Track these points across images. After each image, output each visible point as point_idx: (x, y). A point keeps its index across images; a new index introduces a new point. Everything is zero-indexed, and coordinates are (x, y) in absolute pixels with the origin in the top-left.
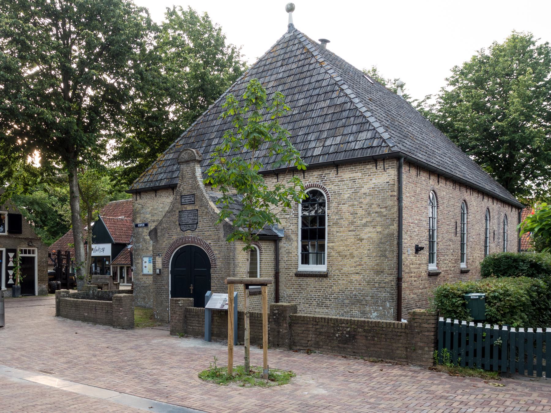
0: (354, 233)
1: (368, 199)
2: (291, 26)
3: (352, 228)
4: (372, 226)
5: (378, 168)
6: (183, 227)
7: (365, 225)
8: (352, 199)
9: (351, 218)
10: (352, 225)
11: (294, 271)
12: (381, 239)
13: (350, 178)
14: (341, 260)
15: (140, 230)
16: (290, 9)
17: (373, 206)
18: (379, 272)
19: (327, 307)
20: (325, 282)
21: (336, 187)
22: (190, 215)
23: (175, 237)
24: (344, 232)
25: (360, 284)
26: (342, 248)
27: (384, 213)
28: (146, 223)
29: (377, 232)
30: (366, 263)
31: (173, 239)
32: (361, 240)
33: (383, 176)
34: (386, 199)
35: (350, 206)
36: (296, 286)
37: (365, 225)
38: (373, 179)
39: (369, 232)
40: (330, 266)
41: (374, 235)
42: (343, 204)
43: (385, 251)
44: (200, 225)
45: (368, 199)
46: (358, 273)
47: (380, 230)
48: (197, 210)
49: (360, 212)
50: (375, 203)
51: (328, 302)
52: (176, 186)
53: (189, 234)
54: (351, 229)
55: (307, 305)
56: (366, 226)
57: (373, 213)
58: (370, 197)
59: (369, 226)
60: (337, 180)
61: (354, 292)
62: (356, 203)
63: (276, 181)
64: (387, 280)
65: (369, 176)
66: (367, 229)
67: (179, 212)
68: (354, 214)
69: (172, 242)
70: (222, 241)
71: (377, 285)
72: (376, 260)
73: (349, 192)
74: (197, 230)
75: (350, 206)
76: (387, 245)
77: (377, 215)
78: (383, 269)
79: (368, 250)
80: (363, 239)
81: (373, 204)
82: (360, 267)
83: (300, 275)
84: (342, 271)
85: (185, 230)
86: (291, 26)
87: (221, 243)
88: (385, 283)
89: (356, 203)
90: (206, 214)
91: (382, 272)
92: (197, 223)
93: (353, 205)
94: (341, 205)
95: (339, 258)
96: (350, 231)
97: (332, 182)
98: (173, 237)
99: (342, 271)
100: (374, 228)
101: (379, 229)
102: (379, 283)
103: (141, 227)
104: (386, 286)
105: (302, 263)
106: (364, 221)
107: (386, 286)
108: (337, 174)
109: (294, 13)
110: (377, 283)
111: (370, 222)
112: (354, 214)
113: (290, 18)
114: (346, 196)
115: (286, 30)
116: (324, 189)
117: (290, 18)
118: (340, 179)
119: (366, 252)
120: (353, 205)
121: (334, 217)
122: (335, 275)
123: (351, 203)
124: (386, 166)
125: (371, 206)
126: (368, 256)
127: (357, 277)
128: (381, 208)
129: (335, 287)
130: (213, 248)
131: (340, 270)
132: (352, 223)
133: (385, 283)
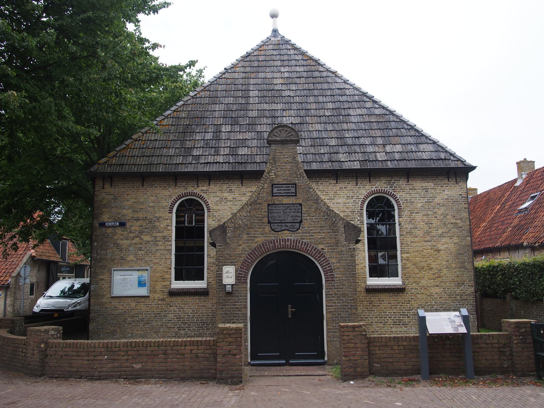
0: (430, 243)
1: (442, 210)
2: (275, 31)
3: (428, 238)
4: (448, 237)
5: (450, 180)
6: (275, 226)
7: (441, 236)
8: (425, 208)
9: (426, 228)
10: (428, 235)
11: (363, 285)
12: (459, 250)
13: (422, 187)
14: (418, 272)
15: (110, 230)
16: (274, 16)
17: (448, 217)
18: (459, 284)
19: (405, 324)
20: (401, 298)
21: (408, 195)
22: (288, 211)
23: (260, 240)
24: (419, 242)
25: (440, 298)
26: (417, 259)
27: (460, 225)
28: (122, 221)
29: (454, 243)
30: (445, 274)
31: (256, 243)
32: (439, 251)
33: (456, 188)
34: (461, 210)
35: (424, 215)
36: (365, 303)
37: (441, 236)
38: (446, 190)
39: (446, 243)
40: (405, 277)
41: (451, 246)
42: (416, 213)
43: (464, 263)
44: (305, 224)
45: (442, 210)
46: (438, 286)
47: (457, 241)
48: (301, 205)
49: (435, 222)
50: (450, 214)
51: (406, 320)
52: (263, 174)
53: (286, 235)
54: (426, 239)
55: (382, 325)
56: (443, 237)
57: (449, 223)
58: (445, 208)
59: (445, 237)
60: (407, 187)
61: (435, 307)
62: (430, 213)
63: (335, 182)
64: (468, 292)
65: (441, 187)
66: (444, 240)
67: (269, 205)
68: (429, 223)
69: (254, 246)
70: (343, 246)
71: (458, 298)
72: (456, 272)
73: (422, 201)
74: (299, 231)
75: (424, 215)
76: (466, 256)
77: (452, 226)
78: (464, 281)
79: (447, 261)
80: (440, 250)
81: (447, 215)
82: (439, 279)
83: (174, 293)
84: (421, 284)
85: (278, 229)
86: (275, 31)
87: (340, 248)
88: (467, 295)
89: (430, 213)
90: (316, 211)
91: (463, 284)
92: (301, 221)
93: (427, 215)
94: (414, 214)
95: (416, 270)
96: (426, 241)
97: (403, 190)
98: (256, 240)
99: (421, 284)
100: (450, 239)
101: (455, 240)
102: (461, 295)
103: (112, 226)
104: (468, 299)
105: (176, 279)
106: (440, 231)
107: (468, 299)
108: (408, 182)
109: (278, 20)
110: (458, 295)
111: (446, 232)
112: (429, 223)
113: (274, 23)
114: (419, 205)
115: (269, 33)
116: (394, 196)
117: (274, 23)
118: (411, 187)
119: (444, 263)
120: (427, 215)
121: (407, 226)
122: (413, 289)
123: (424, 213)
124: (458, 180)
125: (446, 217)
126: (447, 268)
127: (437, 290)
128: (456, 219)
129: (413, 302)
130: (327, 256)
131: (417, 283)
132: (428, 233)
133: (467, 295)
